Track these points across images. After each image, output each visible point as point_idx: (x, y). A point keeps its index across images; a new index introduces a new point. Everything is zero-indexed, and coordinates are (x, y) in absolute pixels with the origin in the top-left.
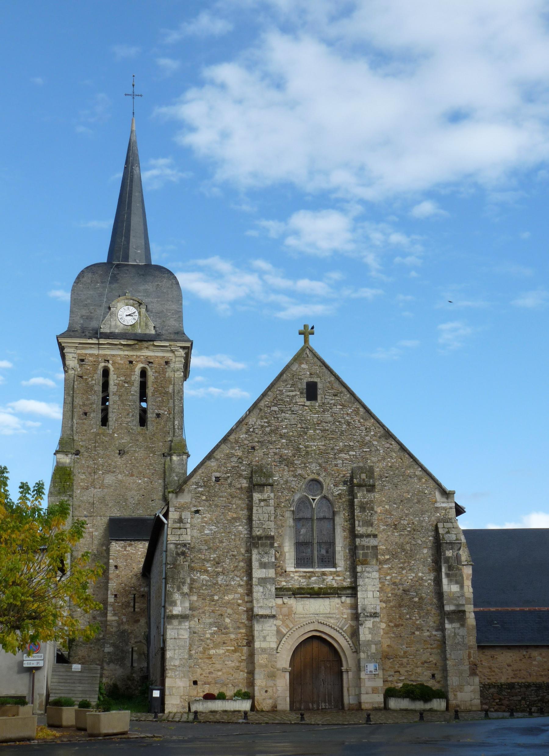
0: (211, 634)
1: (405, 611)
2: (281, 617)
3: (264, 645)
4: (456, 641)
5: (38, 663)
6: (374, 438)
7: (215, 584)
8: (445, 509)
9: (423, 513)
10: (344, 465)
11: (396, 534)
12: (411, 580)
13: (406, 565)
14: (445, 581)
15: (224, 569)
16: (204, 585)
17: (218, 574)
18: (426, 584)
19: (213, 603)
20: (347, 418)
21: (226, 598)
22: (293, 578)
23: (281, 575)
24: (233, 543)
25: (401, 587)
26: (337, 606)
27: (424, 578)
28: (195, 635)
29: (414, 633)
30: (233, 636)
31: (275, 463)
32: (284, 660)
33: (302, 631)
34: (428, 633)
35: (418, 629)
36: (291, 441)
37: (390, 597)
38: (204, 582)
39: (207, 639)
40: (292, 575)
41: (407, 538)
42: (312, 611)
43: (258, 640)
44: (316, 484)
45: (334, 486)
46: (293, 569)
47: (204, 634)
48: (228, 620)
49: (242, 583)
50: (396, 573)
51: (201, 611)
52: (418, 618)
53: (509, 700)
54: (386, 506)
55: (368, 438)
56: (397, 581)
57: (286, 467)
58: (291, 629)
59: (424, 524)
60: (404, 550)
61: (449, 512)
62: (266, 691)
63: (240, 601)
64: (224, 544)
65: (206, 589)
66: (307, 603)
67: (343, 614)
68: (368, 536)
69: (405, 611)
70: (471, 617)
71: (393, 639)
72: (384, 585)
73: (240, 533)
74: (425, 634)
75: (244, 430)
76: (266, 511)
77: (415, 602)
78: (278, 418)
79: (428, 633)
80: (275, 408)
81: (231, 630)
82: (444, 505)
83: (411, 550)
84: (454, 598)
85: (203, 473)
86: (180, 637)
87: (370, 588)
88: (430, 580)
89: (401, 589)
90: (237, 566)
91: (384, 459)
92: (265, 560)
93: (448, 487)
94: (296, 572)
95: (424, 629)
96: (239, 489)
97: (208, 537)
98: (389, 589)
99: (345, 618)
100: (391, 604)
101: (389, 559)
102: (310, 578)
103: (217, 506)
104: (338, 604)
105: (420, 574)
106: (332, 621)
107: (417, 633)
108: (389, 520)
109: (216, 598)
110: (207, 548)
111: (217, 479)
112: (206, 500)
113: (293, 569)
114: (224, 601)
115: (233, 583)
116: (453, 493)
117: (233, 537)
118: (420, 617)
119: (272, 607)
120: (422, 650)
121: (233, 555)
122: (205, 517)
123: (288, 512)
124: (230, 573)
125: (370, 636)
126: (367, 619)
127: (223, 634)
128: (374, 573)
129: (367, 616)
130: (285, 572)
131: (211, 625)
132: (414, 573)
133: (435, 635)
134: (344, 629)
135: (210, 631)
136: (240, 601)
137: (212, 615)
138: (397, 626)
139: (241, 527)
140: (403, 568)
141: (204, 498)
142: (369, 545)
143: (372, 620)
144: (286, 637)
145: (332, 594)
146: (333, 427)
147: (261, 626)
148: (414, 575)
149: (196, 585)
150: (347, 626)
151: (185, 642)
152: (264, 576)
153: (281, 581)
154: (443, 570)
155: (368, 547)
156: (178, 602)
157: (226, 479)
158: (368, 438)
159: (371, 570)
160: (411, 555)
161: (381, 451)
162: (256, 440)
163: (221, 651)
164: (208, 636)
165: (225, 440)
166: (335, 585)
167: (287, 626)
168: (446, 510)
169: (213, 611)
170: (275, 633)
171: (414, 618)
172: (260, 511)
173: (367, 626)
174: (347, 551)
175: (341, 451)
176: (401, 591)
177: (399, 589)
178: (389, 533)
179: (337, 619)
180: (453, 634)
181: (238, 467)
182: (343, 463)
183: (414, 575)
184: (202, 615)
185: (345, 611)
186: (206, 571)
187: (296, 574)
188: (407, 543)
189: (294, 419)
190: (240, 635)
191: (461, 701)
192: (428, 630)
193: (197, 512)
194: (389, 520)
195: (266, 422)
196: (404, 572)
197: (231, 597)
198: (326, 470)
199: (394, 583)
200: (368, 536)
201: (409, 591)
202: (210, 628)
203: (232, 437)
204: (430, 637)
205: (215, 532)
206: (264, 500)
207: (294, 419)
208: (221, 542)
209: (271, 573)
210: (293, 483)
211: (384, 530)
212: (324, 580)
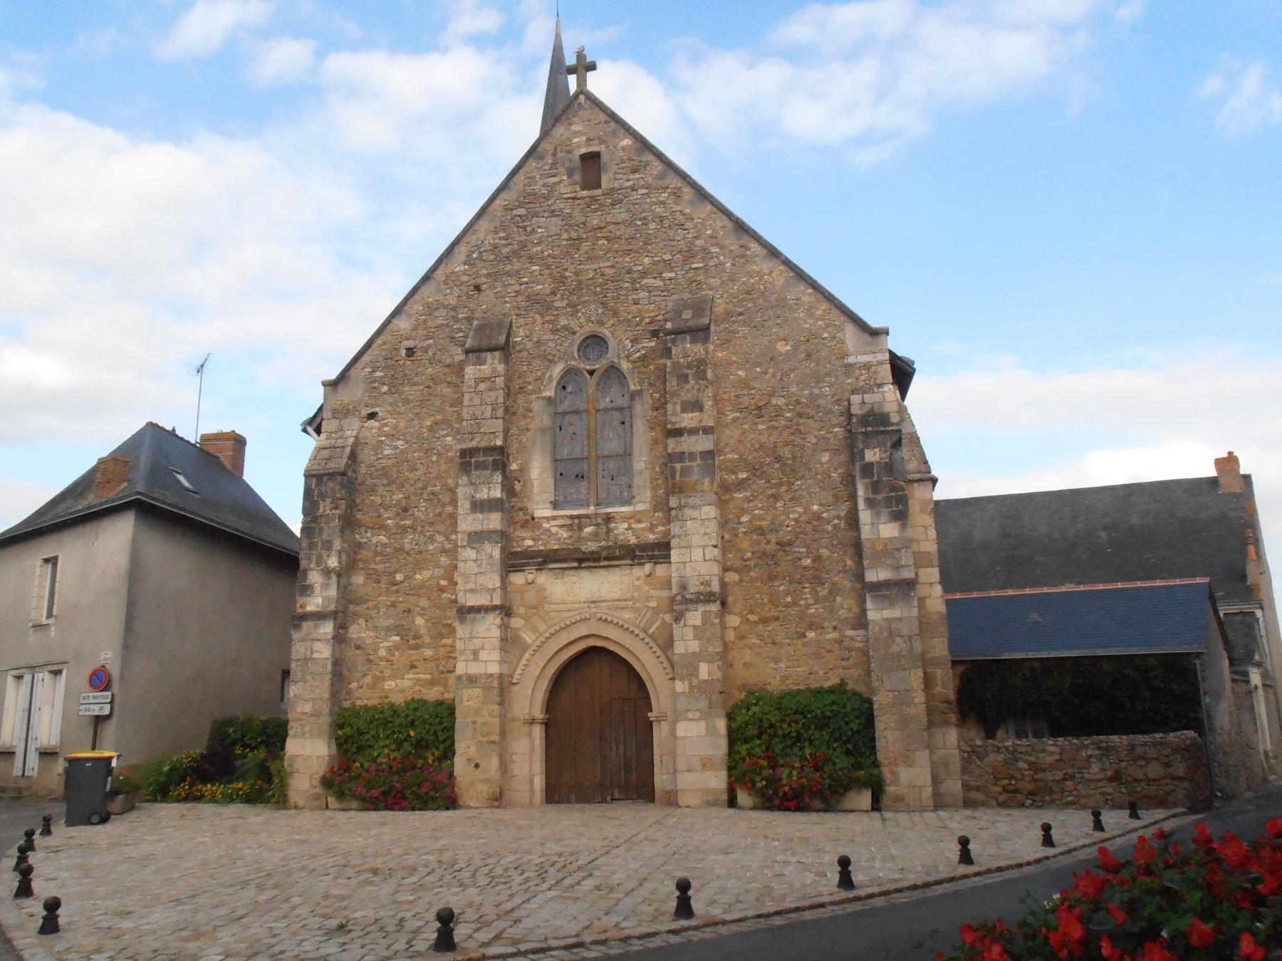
0: (389, 650)
1: (782, 588)
2: (522, 610)
3: (474, 669)
4: (895, 649)
5: (101, 709)
6: (714, 241)
7: (397, 550)
8: (867, 367)
9: (818, 378)
10: (650, 303)
11: (761, 427)
12: (796, 520)
13: (783, 489)
14: (865, 516)
15: (415, 520)
16: (377, 554)
17: (404, 530)
18: (829, 528)
19: (395, 588)
20: (659, 210)
21: (418, 576)
22: (548, 530)
23: (523, 527)
24: (434, 470)
25: (773, 538)
26: (637, 583)
27: (825, 515)
28: (358, 652)
29: (804, 635)
30: (428, 653)
31: (517, 311)
32: (530, 699)
33: (564, 638)
34: (836, 635)
35: (811, 626)
36: (548, 267)
37: (749, 559)
38: (379, 549)
39: (381, 659)
40: (546, 525)
41: (785, 434)
42: (585, 595)
43: (463, 658)
44: (594, 342)
45: (632, 341)
46: (548, 513)
47: (376, 651)
48: (419, 621)
49: (448, 546)
50: (762, 509)
51: (370, 604)
52: (811, 601)
53: (1034, 780)
54: (740, 373)
55: (700, 243)
56: (764, 524)
57: (538, 317)
58: (541, 634)
59: (822, 402)
60: (778, 459)
61: (875, 373)
62: (477, 766)
63: (443, 583)
64: (419, 473)
65: (381, 562)
66: (575, 579)
67: (648, 599)
68: (692, 432)
69: (782, 588)
70: (934, 595)
71: (758, 650)
72: (736, 535)
73: (448, 448)
74: (828, 637)
75: (462, 257)
76: (488, 400)
77: (805, 568)
78: (525, 228)
79: (836, 635)
80: (522, 211)
81: (427, 639)
82: (863, 359)
83: (794, 458)
84: (888, 552)
85: (384, 344)
86: (315, 655)
87: (696, 540)
88: (838, 517)
89: (774, 541)
90: (440, 515)
91: (732, 280)
92: (483, 494)
93: (874, 323)
94: (554, 518)
95: (826, 624)
96: (448, 366)
97: (391, 462)
98: (745, 544)
99: (653, 608)
100: (752, 574)
101: (747, 479)
102: (580, 528)
103: (406, 401)
104: (638, 579)
105: (815, 507)
106: (626, 615)
107: (811, 635)
108: (746, 399)
109: (399, 577)
110: (385, 482)
111: (410, 352)
112: (390, 393)
113: (548, 513)
114: (414, 583)
115: (431, 547)
116: (886, 332)
117: (434, 458)
118: (817, 602)
119: (494, 590)
120: (821, 673)
121: (433, 494)
122: (386, 425)
123: (540, 402)
124: (427, 528)
125: (697, 642)
126: (690, 606)
127: (411, 648)
128: (706, 509)
129: (691, 601)
130: (533, 519)
131: (388, 630)
132: (800, 504)
133: (852, 639)
134: (651, 631)
135: (386, 644)
136: (443, 583)
137: (392, 611)
138: (765, 621)
139: (449, 439)
140: (776, 497)
141: (385, 389)
142: (693, 449)
143: (701, 608)
144: (531, 651)
145: (621, 558)
146: (630, 231)
147: (468, 631)
148: (800, 510)
149: (364, 554)
150: (657, 624)
151: (325, 666)
152: (479, 528)
153: (524, 539)
154: (861, 492)
155: (692, 456)
156: (317, 588)
157: (426, 350)
158: (700, 243)
159: (699, 502)
160: (792, 469)
161: (728, 265)
162: (484, 271)
163: (407, 683)
164: (382, 653)
165: (426, 279)
166: (633, 540)
167: (534, 629)
168: (868, 369)
169: (393, 605)
170: (497, 643)
171: (803, 602)
172: (477, 401)
173: (690, 622)
174: (657, 469)
175: (644, 274)
176: (772, 547)
177: (768, 542)
178: (746, 427)
179: (636, 610)
180: (886, 634)
181: (447, 325)
182: (649, 297)
183: (800, 510)
184: (373, 613)
185: (652, 593)
186: (383, 527)
187: (553, 523)
188: (787, 443)
189: (556, 225)
190: (442, 650)
191: (909, 787)
192: (835, 628)
193: (372, 416)
194: (746, 399)
195: (503, 238)
196: (778, 505)
197: (427, 574)
198: (615, 313)
199: (760, 531)
200: (692, 432)
201: (790, 544)
202: (386, 637)
203: (440, 273)
204: (840, 642)
205: (402, 452)
206: (483, 380)
207: (556, 225)
208: (414, 469)
209: (494, 521)
210: (551, 344)
211: (735, 420)
212: (609, 531)
